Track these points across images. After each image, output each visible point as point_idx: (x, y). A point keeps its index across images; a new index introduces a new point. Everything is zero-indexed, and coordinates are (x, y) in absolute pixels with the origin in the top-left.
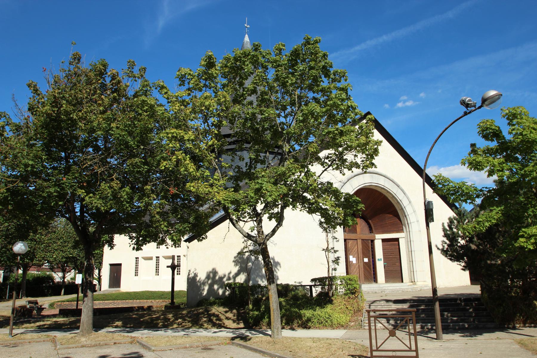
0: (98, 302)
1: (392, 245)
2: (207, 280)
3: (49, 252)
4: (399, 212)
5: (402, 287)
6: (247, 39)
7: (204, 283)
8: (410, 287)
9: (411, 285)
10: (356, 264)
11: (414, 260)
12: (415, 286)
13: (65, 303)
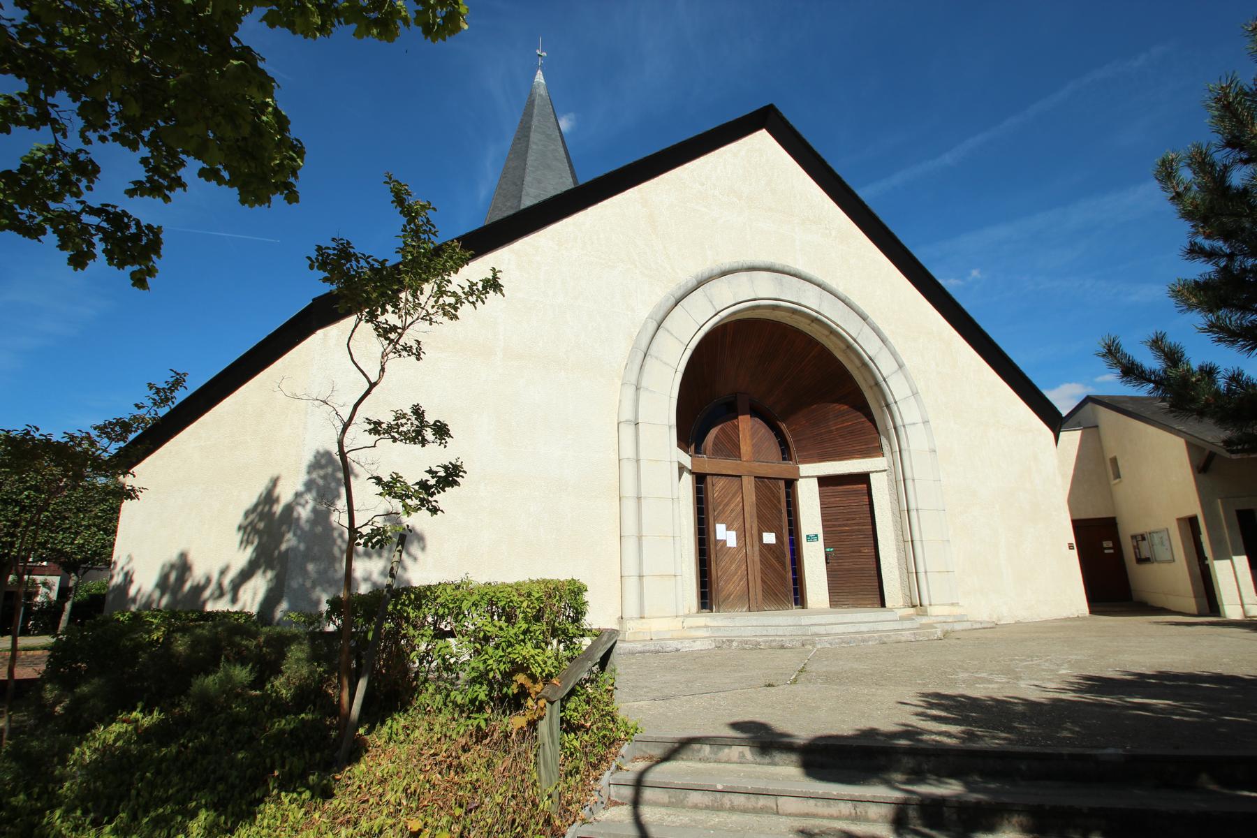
1: (848, 495)
3: (64, 531)
4: (868, 395)
5: (880, 627)
6: (540, 78)
8: (907, 624)
9: (909, 618)
10: (739, 549)
11: (916, 537)
12: (924, 620)
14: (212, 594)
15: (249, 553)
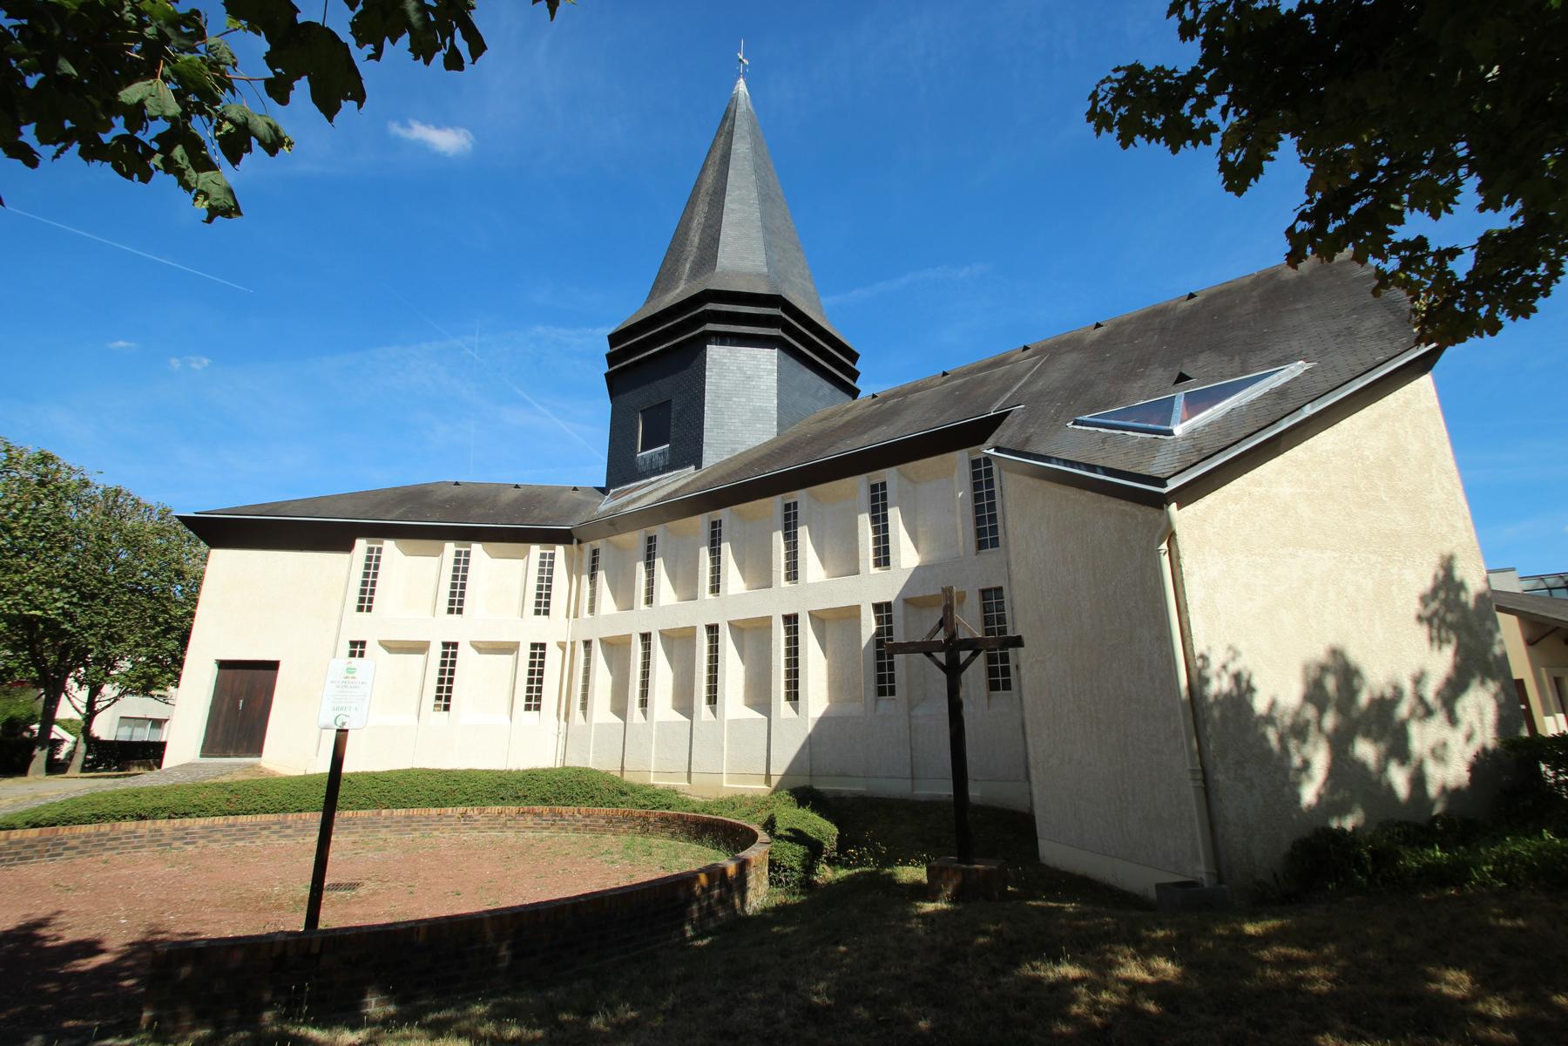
0: (202, 821)
2: (1310, 712)
6: (741, 86)
7: (1299, 731)
13: (16, 835)
14: (1412, 713)
15: (1448, 652)
